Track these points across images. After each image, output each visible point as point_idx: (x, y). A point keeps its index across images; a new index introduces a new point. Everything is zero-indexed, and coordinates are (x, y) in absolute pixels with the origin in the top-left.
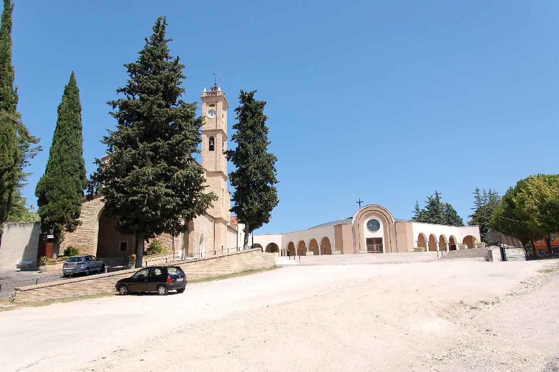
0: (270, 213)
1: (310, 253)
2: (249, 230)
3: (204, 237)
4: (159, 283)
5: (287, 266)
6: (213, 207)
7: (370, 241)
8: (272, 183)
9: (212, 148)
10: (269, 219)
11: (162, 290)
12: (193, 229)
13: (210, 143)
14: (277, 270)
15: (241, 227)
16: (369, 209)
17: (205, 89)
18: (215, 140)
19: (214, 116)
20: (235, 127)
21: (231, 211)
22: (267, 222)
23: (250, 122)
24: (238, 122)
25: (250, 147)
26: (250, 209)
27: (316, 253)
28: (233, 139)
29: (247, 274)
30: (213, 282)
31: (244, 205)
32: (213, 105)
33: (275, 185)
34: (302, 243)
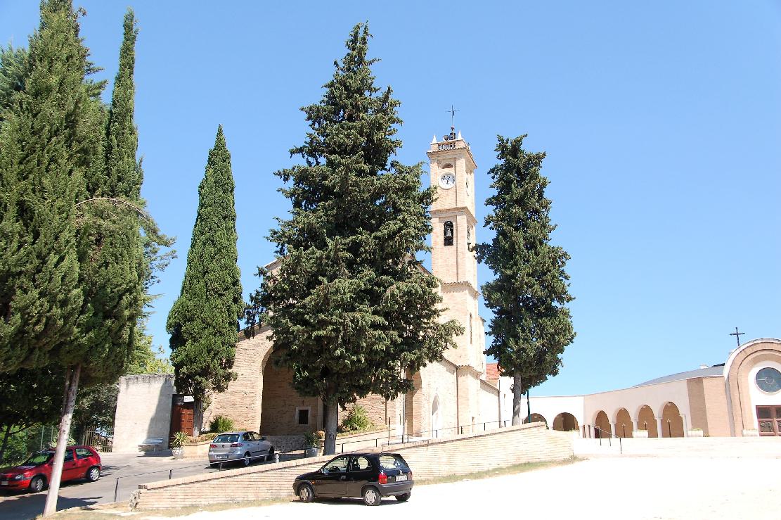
0: (559, 356)
1: (640, 435)
2: (522, 387)
3: (441, 399)
4: (365, 482)
6: (455, 346)
7: (763, 412)
8: (561, 300)
11: (371, 496)
14: (577, 464)
16: (759, 348)
19: (451, 185)
20: (489, 202)
22: (555, 373)
23: (517, 191)
24: (495, 192)
25: (519, 238)
27: (653, 434)
28: (487, 223)
29: (523, 471)
30: (459, 484)
32: (449, 166)
33: (566, 305)
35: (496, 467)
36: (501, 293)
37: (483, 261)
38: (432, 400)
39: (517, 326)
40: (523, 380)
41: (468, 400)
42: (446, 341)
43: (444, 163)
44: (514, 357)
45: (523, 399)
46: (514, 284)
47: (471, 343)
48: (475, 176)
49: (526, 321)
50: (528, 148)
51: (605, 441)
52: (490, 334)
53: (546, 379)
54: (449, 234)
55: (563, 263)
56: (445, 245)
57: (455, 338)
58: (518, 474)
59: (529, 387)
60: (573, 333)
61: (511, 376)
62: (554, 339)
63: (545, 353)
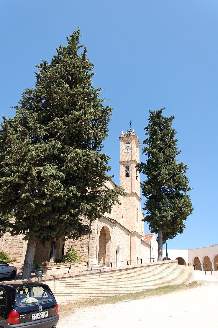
0: (184, 221)
2: (163, 239)
3: (121, 247)
5: (209, 282)
6: (120, 203)
8: (185, 190)
9: (127, 175)
10: (184, 228)
12: (109, 239)
13: (126, 171)
14: (199, 288)
15: (155, 236)
17: (123, 132)
18: (130, 167)
19: (129, 151)
20: (145, 142)
21: (144, 220)
22: (181, 232)
23: (160, 135)
24: (148, 137)
25: (161, 155)
26: (163, 216)
28: (144, 152)
29: (165, 293)
30: (121, 305)
31: (157, 212)
32: (128, 143)
33: (188, 193)
34: (206, 259)
35: (148, 288)
36: (151, 185)
37: (142, 172)
38: (116, 247)
39: (160, 203)
40: (164, 235)
41: (135, 248)
42: (114, 200)
43: (126, 142)
44: (158, 220)
45: (164, 245)
46: (158, 179)
47: (137, 221)
48: (140, 149)
49: (165, 200)
50: (164, 115)
51: (208, 272)
52: (145, 209)
53: (177, 235)
54: (128, 172)
55: (184, 171)
56: (126, 176)
57: (120, 198)
58: (163, 296)
59: (167, 239)
60: (192, 208)
61: (157, 233)
62: (182, 210)
63: (177, 218)
